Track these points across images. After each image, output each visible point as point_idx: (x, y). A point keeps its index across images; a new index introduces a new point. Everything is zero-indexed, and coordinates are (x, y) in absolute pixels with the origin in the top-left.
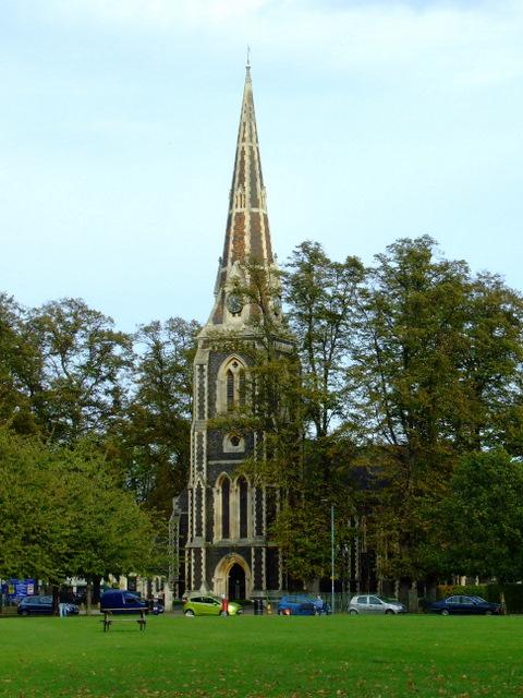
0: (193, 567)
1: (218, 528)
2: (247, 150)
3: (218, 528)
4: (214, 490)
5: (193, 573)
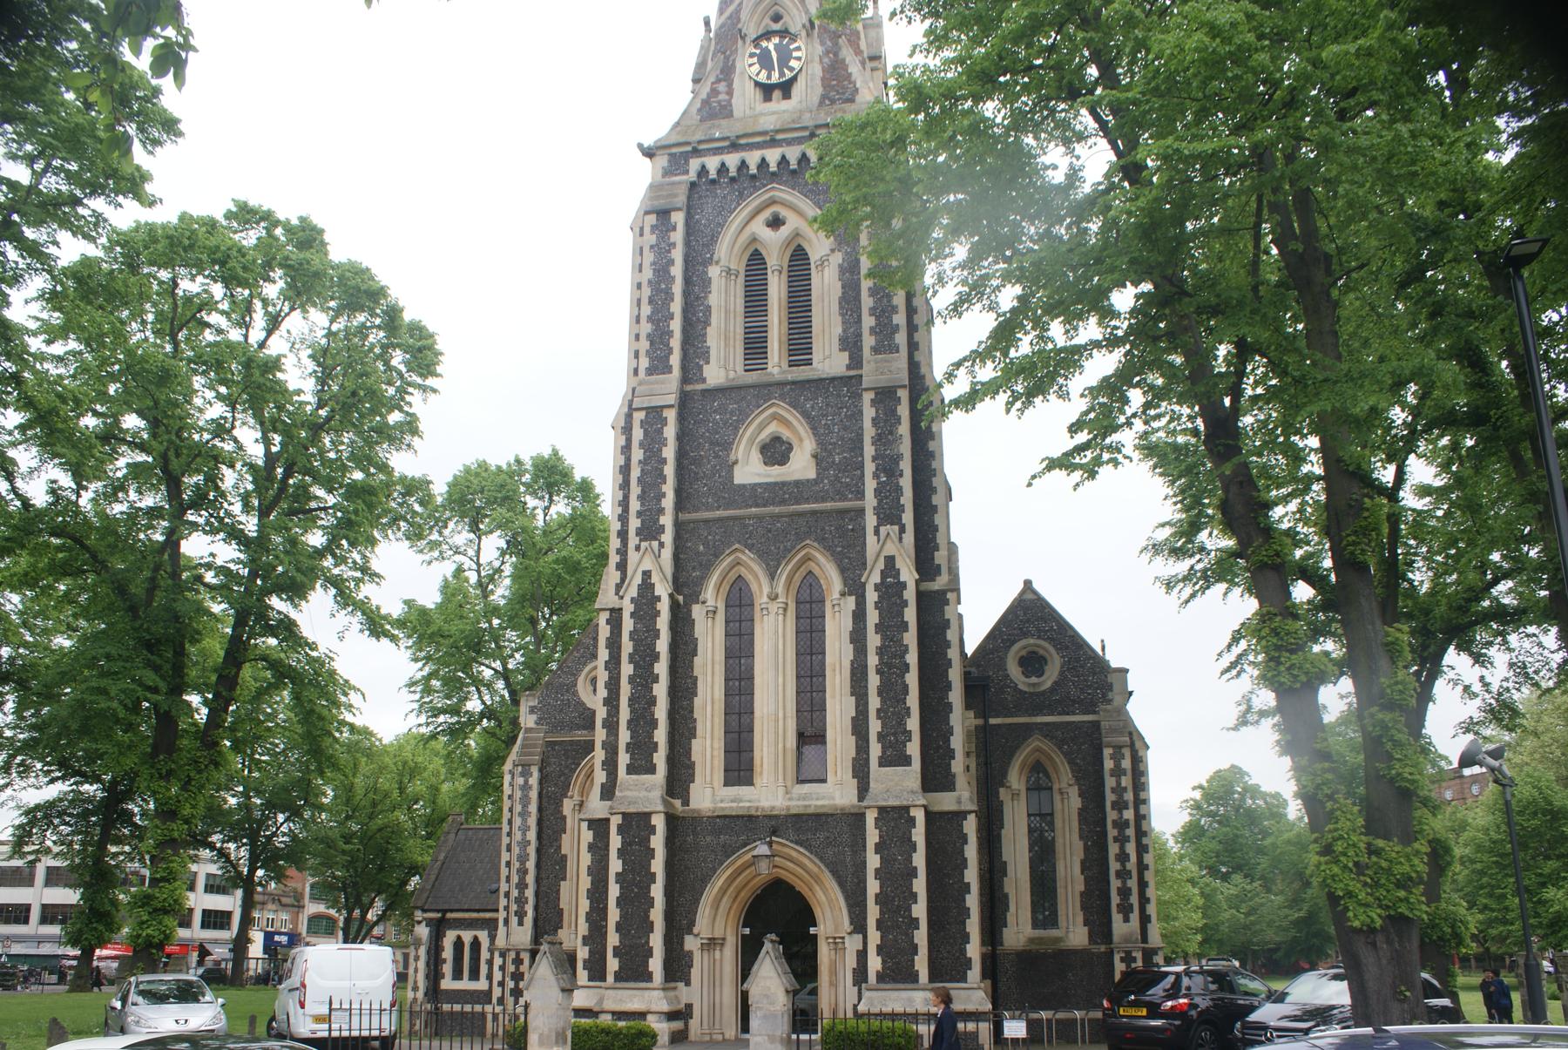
0: (614, 891)
1: (708, 748)
2: (775, 260)
3: (708, 748)
4: (697, 612)
5: (614, 915)
